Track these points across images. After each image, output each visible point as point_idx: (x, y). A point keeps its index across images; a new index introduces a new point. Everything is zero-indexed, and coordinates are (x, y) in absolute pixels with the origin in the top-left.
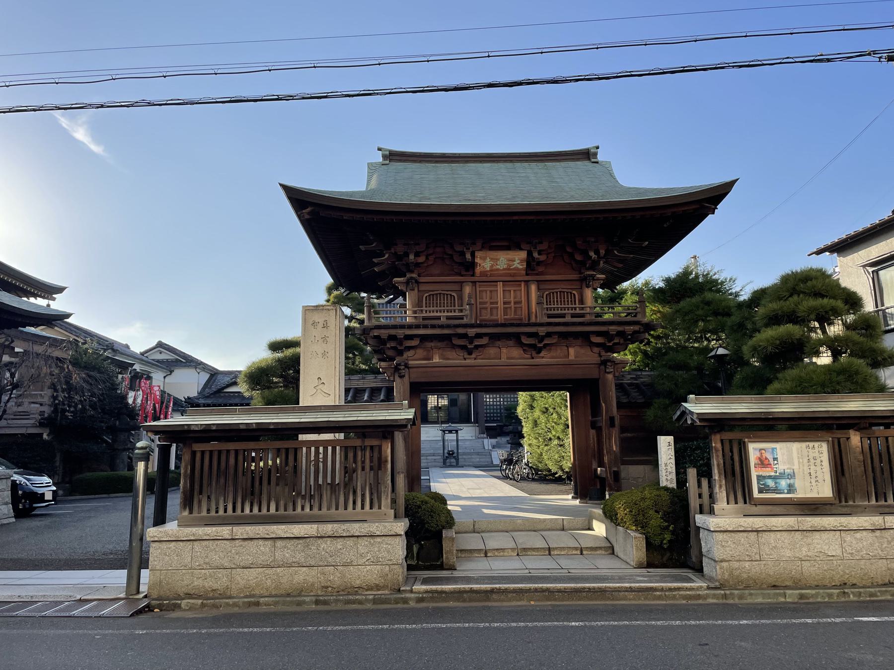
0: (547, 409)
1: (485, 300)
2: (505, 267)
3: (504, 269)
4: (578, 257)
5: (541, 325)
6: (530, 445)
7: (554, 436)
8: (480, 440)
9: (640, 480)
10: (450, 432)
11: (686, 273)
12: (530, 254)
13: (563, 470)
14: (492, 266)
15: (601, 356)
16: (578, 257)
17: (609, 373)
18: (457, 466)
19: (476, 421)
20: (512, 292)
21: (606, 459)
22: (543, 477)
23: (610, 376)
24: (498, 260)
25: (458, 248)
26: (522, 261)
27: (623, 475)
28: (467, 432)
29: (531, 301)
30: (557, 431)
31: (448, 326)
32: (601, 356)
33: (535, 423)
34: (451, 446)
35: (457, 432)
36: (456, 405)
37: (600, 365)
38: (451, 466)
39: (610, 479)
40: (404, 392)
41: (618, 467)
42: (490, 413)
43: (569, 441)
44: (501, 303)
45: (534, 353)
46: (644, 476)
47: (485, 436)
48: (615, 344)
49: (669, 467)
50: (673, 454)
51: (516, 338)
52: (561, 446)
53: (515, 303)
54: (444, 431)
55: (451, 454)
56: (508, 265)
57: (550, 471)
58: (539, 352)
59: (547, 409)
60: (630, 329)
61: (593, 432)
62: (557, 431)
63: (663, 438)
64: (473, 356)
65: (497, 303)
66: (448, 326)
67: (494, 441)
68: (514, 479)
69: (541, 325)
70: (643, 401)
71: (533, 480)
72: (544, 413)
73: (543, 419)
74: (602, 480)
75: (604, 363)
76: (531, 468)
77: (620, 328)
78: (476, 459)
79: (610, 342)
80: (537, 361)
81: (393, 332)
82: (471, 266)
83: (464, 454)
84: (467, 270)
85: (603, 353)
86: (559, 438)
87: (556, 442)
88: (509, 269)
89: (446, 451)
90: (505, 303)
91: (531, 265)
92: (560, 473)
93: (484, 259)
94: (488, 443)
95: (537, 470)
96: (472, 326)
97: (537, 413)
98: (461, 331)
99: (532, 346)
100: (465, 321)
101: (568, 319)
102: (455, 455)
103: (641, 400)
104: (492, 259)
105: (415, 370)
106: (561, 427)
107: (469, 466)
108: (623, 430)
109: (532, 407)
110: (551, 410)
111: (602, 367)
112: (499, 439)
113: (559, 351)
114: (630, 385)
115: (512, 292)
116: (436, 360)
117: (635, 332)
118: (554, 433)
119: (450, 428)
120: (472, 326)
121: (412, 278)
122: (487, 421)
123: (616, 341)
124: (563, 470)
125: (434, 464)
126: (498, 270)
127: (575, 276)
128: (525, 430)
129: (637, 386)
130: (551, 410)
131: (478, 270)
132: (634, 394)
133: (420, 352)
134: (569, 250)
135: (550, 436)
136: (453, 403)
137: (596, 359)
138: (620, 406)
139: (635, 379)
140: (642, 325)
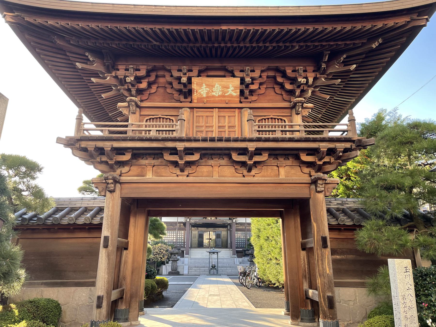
0: (268, 237)
1: (201, 124)
2: (220, 93)
3: (219, 96)
4: (288, 86)
5: (251, 140)
6: (258, 263)
7: (273, 257)
8: (233, 259)
9: (351, 303)
10: (214, 253)
11: (380, 118)
12: (242, 81)
13: (279, 282)
14: (207, 93)
15: (311, 176)
16: (288, 86)
17: (319, 192)
18: (217, 274)
19: (231, 247)
20: (227, 117)
21: (319, 281)
22: (266, 285)
23: (321, 196)
24: (213, 86)
25: (176, 74)
26: (235, 88)
27: (337, 298)
28: (225, 254)
29: (244, 127)
30: (275, 254)
31: (156, 140)
32: (311, 176)
33: (261, 248)
34: (214, 262)
35: (217, 253)
36: (220, 237)
37: (311, 184)
38: (214, 274)
39: (324, 305)
40: (113, 207)
41: (333, 292)
42: (239, 243)
43: (282, 262)
44: (215, 126)
45: (245, 172)
46: (356, 299)
47: (236, 256)
48: (325, 163)
49: (407, 301)
50: (412, 283)
51: (226, 153)
52: (278, 264)
53: (229, 127)
54: (210, 253)
55: (214, 267)
56: (223, 91)
57: (271, 282)
58: (250, 170)
59: (268, 237)
60: (340, 146)
61: (303, 254)
62: (275, 254)
63: (397, 261)
64: (186, 173)
65: (212, 127)
66: (156, 140)
67: (240, 259)
68: (246, 286)
69: (251, 140)
70: (351, 223)
71: (260, 287)
72: (266, 240)
73: (265, 245)
74: (315, 304)
75: (314, 182)
76: (258, 279)
77: (331, 145)
78: (229, 271)
79: (320, 160)
80: (248, 179)
81: (100, 144)
82: (187, 93)
83: (222, 267)
84: (186, 98)
85: (313, 173)
86: (276, 259)
87: (274, 261)
88: (224, 96)
89: (211, 265)
90: (219, 127)
91: (246, 92)
92: (277, 284)
93: (200, 85)
94: (238, 260)
95: (263, 282)
96: (181, 140)
97: (262, 241)
98: (170, 145)
99: (243, 164)
100: (175, 135)
101: (278, 135)
102: (216, 267)
103: (349, 222)
104: (208, 86)
105: (127, 185)
106: (278, 250)
107: (225, 274)
108: (333, 252)
109: (259, 237)
110: (271, 238)
111: (313, 187)
112: (243, 258)
113: (270, 171)
114: (338, 210)
115: (227, 117)
116: (150, 176)
117: (346, 150)
118: (273, 255)
119: (213, 251)
120: (181, 140)
121: (133, 101)
122: (237, 248)
123: (327, 159)
124: (279, 282)
125: (204, 273)
126: (213, 96)
127: (286, 105)
128: (255, 253)
129: (344, 211)
130: (271, 238)
131: (195, 96)
132: (342, 217)
133: (135, 169)
134: (280, 80)
135: (270, 257)
136: (218, 236)
137: (307, 179)
138: (331, 228)
139: (342, 204)
140: (353, 141)
